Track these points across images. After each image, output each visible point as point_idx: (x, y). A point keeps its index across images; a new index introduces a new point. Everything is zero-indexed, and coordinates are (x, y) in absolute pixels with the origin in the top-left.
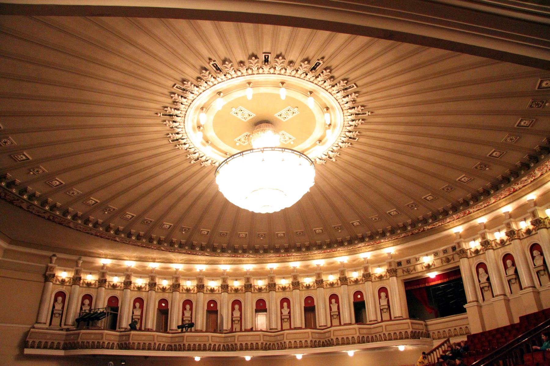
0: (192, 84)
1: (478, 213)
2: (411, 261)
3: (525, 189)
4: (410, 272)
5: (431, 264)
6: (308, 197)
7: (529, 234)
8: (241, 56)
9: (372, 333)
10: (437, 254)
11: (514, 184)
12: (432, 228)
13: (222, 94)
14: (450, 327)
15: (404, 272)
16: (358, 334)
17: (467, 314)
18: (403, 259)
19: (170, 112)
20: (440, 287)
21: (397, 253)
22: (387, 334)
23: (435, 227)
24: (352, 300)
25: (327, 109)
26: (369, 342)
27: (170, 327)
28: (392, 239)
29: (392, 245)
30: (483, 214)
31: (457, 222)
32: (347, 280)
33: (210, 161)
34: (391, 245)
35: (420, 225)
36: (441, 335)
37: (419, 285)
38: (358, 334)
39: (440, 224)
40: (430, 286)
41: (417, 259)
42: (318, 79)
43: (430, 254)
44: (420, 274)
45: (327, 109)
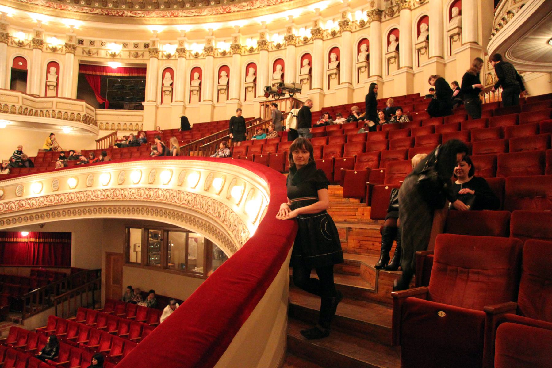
1: (183, 20)
2: (95, 44)
3: (237, 15)
4: (92, 55)
5: (117, 54)
7: (224, 56)
9: (37, 107)
10: (127, 45)
11: (233, 5)
12: (132, 16)
14: (120, 121)
15: (84, 53)
16: (21, 104)
17: (143, 112)
18: (87, 39)
20: (118, 80)
21: (81, 29)
22: (57, 112)
23: (135, 17)
24: (11, 65)
26: (26, 115)
28: (82, 11)
29: (78, 18)
30: (187, 23)
31: (159, 20)
32: (9, 39)
34: (77, 18)
35: (124, 7)
36: (109, 126)
37: (95, 71)
38: (21, 104)
39: (143, 15)
40: (107, 76)
41: (102, 44)
43: (119, 43)
44: (101, 60)
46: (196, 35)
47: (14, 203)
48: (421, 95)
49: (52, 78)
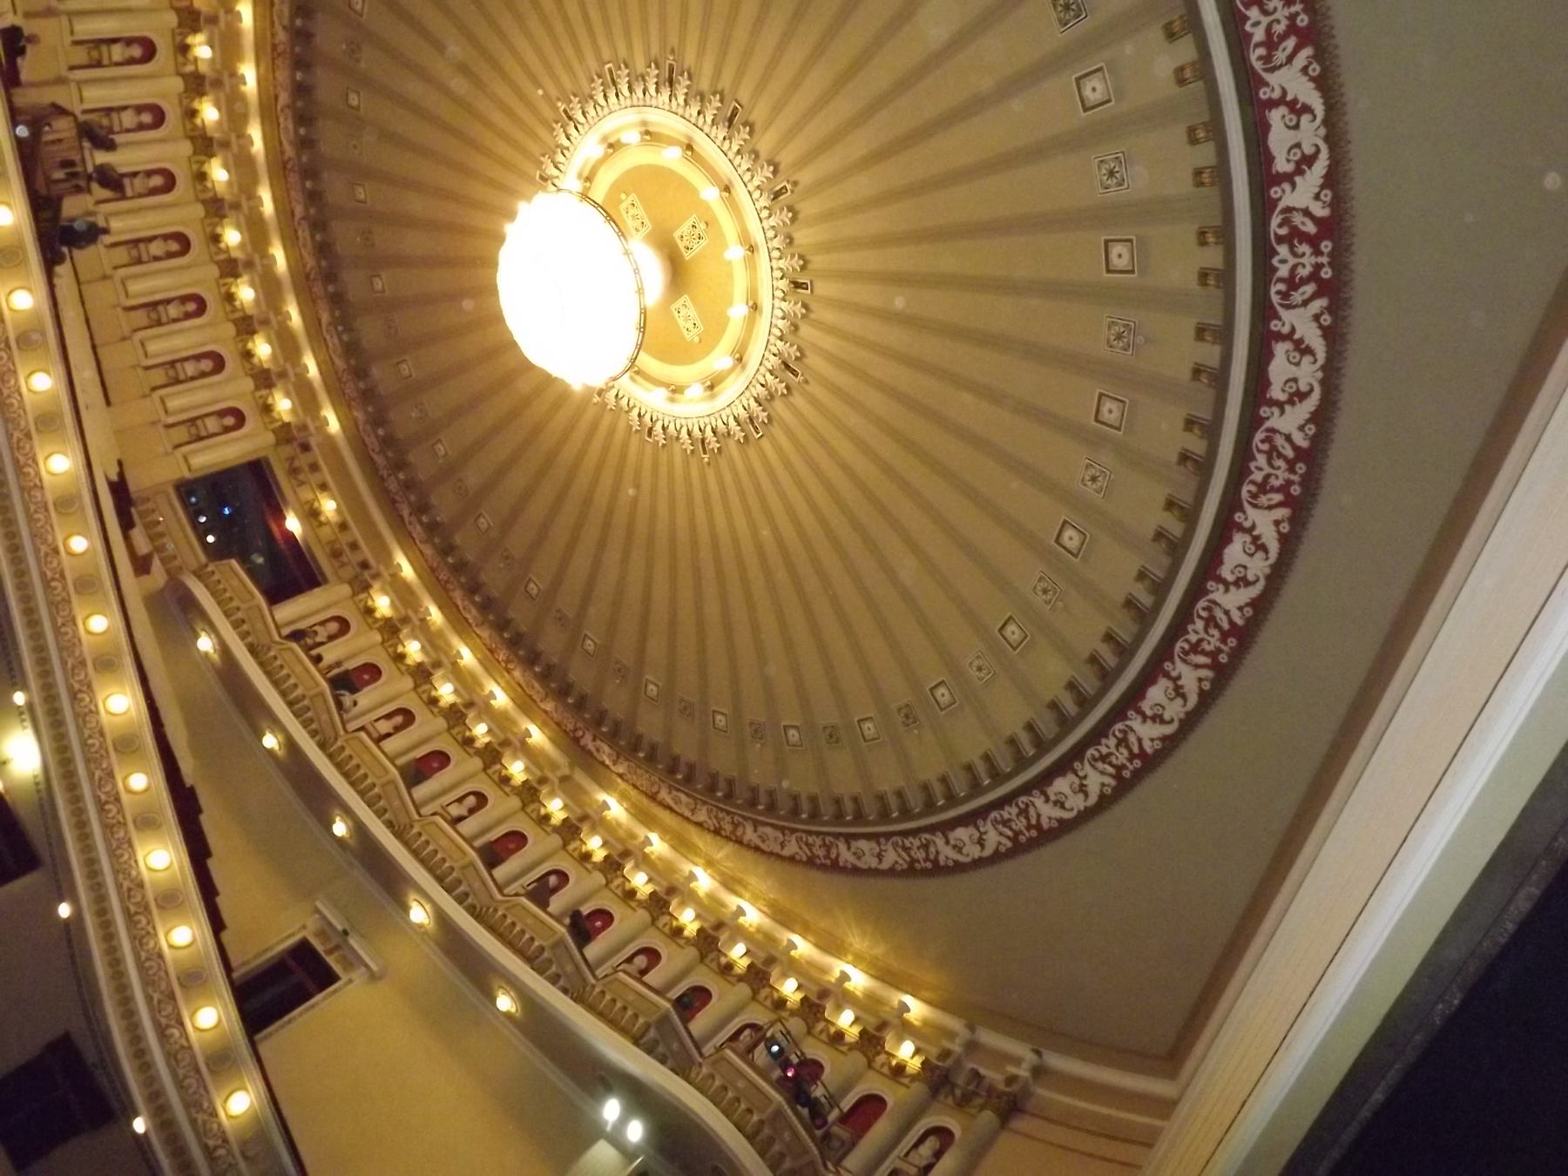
0: (745, 140)
6: (547, 380)
8: (803, 236)
18: (317, 455)
19: (619, 77)
25: (711, 387)
27: (173, 394)
33: (566, 143)
41: (324, 487)
42: (768, 375)
45: (711, 387)
47: (118, 812)
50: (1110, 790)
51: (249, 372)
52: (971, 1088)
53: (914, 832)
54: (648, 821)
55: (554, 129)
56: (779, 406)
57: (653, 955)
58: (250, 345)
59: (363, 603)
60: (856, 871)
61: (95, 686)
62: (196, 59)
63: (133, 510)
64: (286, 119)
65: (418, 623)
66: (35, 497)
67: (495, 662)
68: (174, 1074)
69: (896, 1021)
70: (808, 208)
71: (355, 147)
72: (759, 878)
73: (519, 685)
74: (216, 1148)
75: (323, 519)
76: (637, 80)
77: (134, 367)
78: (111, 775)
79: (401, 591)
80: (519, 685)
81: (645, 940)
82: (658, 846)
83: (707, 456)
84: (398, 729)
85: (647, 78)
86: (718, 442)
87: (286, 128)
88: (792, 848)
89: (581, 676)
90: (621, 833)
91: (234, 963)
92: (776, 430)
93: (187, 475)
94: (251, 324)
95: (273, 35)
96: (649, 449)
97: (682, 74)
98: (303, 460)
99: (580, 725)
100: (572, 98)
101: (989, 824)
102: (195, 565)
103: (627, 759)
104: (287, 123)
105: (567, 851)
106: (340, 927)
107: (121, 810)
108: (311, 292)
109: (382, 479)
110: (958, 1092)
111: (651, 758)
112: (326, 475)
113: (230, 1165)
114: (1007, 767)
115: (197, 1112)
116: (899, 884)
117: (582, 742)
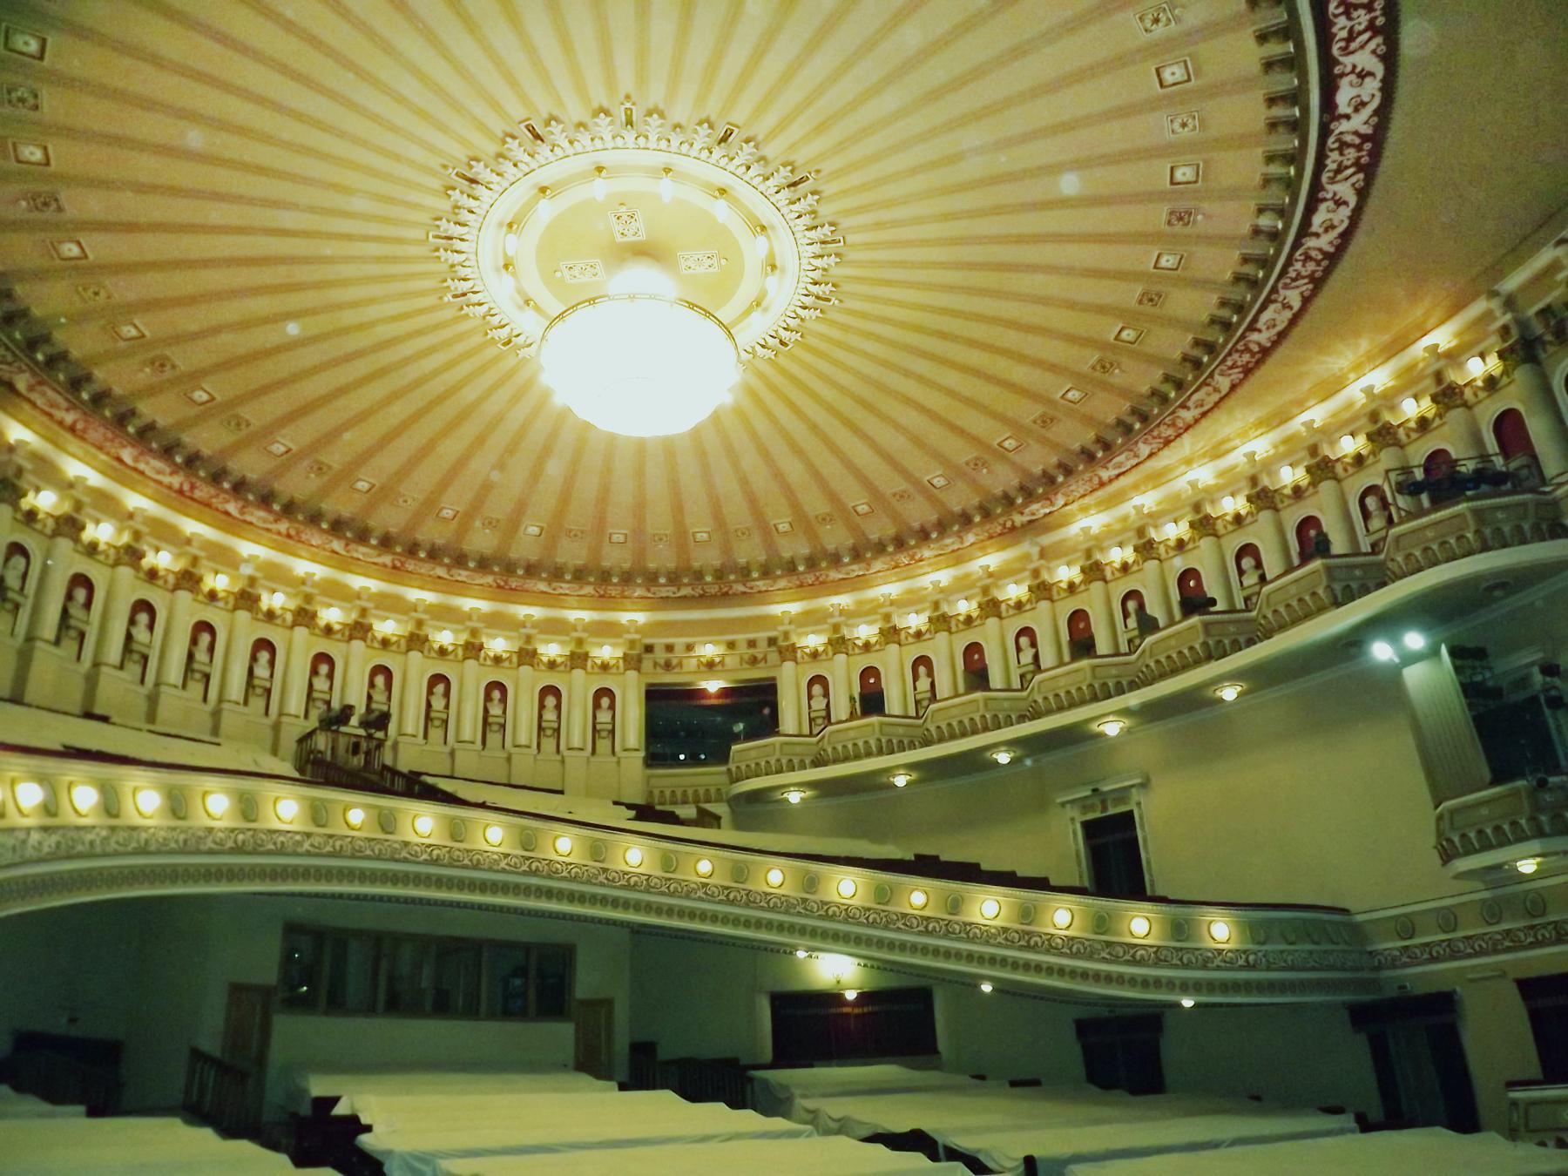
13: (548, 192)
18: (659, 641)
19: (446, 231)
33: (484, 308)
35: (732, 577)
38: (877, 735)
41: (690, 648)
45: (774, 267)
46: (554, 628)
48: (365, 1140)
49: (604, 717)
50: (1383, 47)
51: (568, 669)
52: (1553, 323)
53: (1289, 262)
54: (1119, 498)
55: (467, 315)
56: (826, 211)
57: (1248, 550)
58: (545, 659)
59: (806, 657)
60: (1282, 336)
61: (827, 899)
62: (282, 608)
63: (658, 808)
64: (357, 551)
65: (843, 619)
66: (656, 884)
67: (907, 568)
68: (1175, 966)
69: (1442, 363)
70: (656, 94)
71: (405, 501)
72: (1225, 425)
73: (936, 556)
74: (1247, 960)
75: (717, 660)
76: (457, 214)
77: (535, 760)
78: (904, 915)
79: (810, 620)
80: (936, 556)
81: (1230, 552)
82: (1148, 500)
83: (833, 299)
84: (930, 674)
85: (459, 204)
86: (827, 284)
87: (364, 554)
88: (1224, 383)
89: (960, 499)
90: (1117, 527)
91: (1076, 883)
92: (846, 223)
93: (642, 754)
94: (527, 652)
95: (279, 533)
96: (798, 352)
97: (471, 167)
98: (660, 655)
99: (1001, 520)
100: (445, 284)
101: (1328, 187)
102: (724, 779)
103: (1056, 494)
104: (360, 551)
105: (1111, 581)
106: (1089, 793)
107: (937, 920)
108: (515, 590)
109: (701, 596)
110: (1549, 338)
111: (1068, 471)
112: (679, 642)
113: (1264, 956)
114: (1293, 142)
115: (1213, 962)
116: (1321, 301)
117: (1018, 524)
